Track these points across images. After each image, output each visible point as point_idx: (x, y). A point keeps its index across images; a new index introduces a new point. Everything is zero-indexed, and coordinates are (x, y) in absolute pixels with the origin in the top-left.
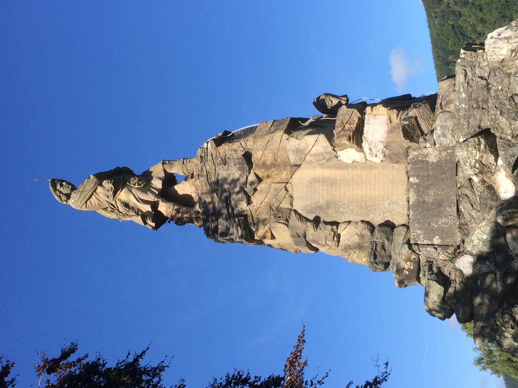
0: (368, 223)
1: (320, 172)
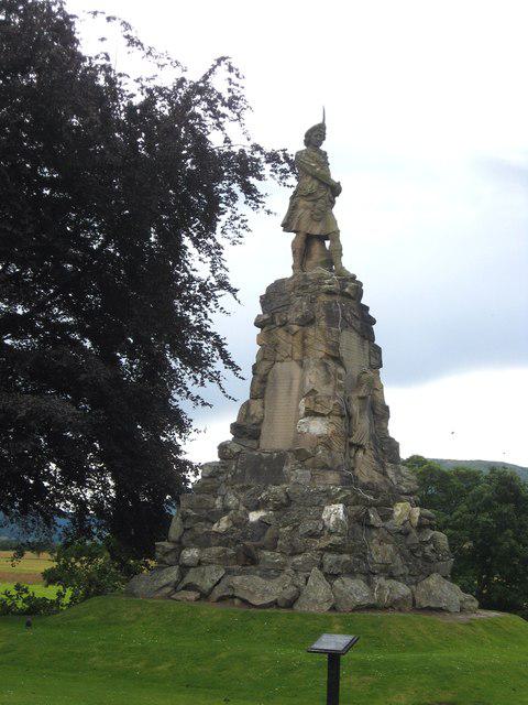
0: (262, 421)
1: (296, 382)
